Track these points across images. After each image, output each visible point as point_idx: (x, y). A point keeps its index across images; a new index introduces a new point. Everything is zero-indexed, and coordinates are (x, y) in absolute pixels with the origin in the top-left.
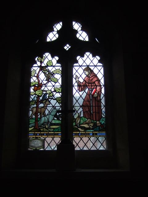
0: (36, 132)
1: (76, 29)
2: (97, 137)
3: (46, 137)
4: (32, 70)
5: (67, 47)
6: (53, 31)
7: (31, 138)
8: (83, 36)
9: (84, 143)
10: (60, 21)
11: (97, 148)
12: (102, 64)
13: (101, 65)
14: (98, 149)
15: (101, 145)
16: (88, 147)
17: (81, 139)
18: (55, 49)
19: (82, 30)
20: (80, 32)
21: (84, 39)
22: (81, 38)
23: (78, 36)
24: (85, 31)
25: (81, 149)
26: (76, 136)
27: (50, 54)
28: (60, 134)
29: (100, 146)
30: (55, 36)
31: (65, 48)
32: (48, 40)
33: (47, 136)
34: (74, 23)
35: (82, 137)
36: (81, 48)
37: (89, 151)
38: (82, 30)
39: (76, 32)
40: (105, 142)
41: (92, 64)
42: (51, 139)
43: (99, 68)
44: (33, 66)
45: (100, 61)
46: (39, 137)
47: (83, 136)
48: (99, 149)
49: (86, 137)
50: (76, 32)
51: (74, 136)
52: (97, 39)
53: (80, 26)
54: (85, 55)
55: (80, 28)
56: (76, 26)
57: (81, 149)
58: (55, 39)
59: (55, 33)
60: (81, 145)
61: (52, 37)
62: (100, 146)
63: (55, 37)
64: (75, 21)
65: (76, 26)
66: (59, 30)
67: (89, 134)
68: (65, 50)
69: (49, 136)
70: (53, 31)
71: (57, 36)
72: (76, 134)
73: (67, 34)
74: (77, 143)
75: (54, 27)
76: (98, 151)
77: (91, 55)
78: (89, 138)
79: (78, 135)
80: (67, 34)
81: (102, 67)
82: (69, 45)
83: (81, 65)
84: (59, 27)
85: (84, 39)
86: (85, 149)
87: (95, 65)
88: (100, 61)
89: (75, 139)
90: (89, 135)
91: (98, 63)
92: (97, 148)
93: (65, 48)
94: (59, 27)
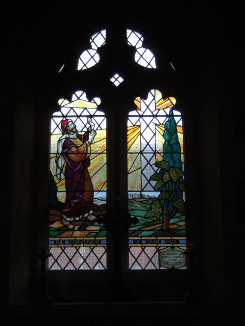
0: (174, 237)
1: (134, 45)
2: (78, 248)
3: (94, 247)
4: (129, 124)
5: (117, 80)
6: (90, 47)
7: (163, 248)
8: (146, 58)
9: (142, 258)
10: (103, 29)
11: (90, 268)
12: (104, 112)
13: (102, 113)
14: (92, 268)
15: (69, 261)
16: (75, 265)
17: (63, 251)
18: (93, 83)
19: (145, 45)
20: (141, 50)
21: (149, 64)
22: (143, 63)
23: (137, 57)
24: (150, 49)
25: (143, 268)
26: (149, 245)
27: (85, 93)
28: (105, 242)
29: (68, 264)
30: (92, 57)
31: (121, 80)
32: (80, 66)
33: (95, 245)
34: (129, 32)
35: (65, 247)
36: (140, 82)
37: (77, 272)
38: (145, 45)
39: (133, 50)
40: (105, 256)
41: (72, 113)
42: (60, 251)
43: (99, 120)
44: (54, 115)
45: (99, 108)
46: (178, 247)
47: (65, 246)
48: (65, 268)
49: (72, 247)
50: (133, 50)
51: (130, 245)
52: (173, 65)
53: (140, 39)
54: (149, 93)
55: (140, 44)
56: (134, 38)
57: (143, 268)
58: (91, 64)
59: (93, 52)
60: (63, 261)
61: (88, 60)
62: (68, 264)
63: (142, 58)
64: (130, 28)
65: (134, 38)
66: (99, 46)
67: (134, 241)
68: (121, 84)
69: (98, 245)
70: (90, 47)
71: (97, 58)
72: (136, 242)
73: (117, 55)
74: (136, 258)
75: (91, 41)
76: (92, 272)
77: (84, 96)
78: (63, 248)
79: (140, 243)
80: (117, 55)
81: (104, 117)
82: (111, 78)
83: (79, 114)
84: (99, 40)
85: (149, 64)
86: (70, 268)
87: (79, 114)
88: (99, 108)
89: (133, 250)
90: (64, 244)
91: (98, 111)
92: (90, 268)
93: (121, 80)
94: (99, 40)
